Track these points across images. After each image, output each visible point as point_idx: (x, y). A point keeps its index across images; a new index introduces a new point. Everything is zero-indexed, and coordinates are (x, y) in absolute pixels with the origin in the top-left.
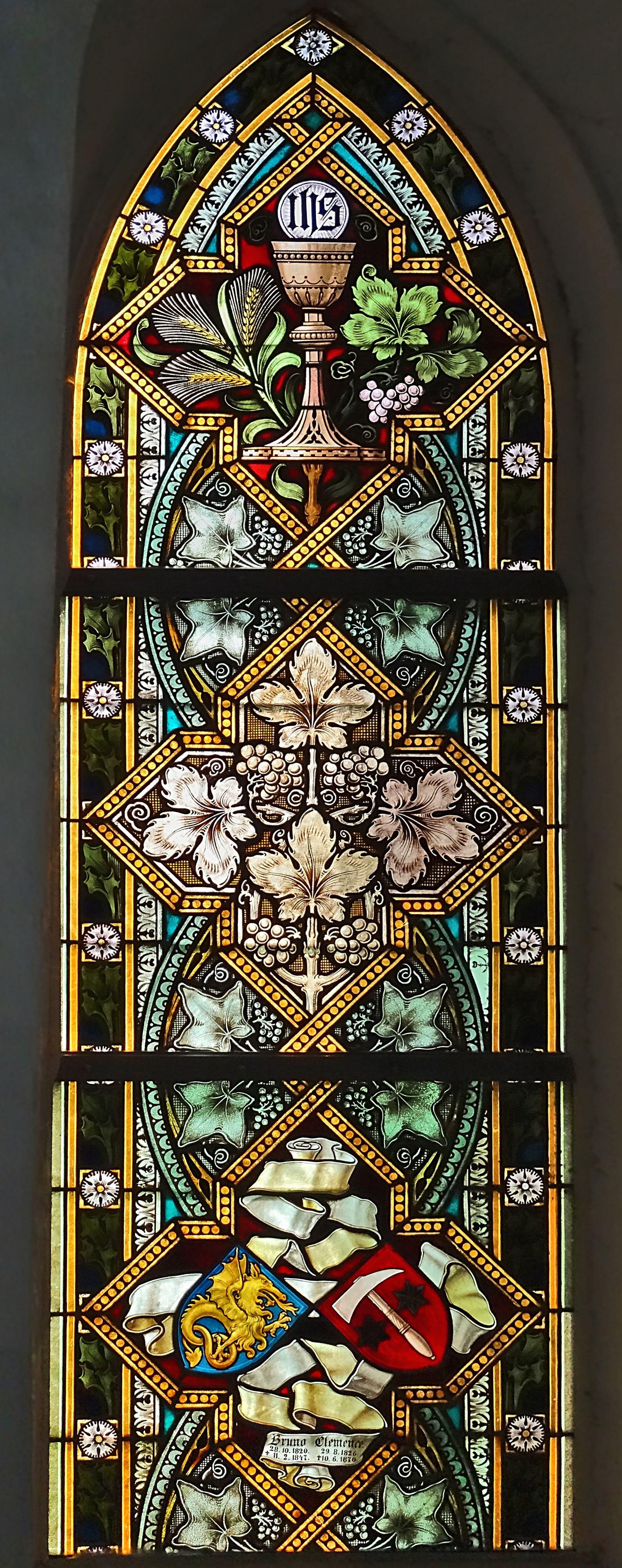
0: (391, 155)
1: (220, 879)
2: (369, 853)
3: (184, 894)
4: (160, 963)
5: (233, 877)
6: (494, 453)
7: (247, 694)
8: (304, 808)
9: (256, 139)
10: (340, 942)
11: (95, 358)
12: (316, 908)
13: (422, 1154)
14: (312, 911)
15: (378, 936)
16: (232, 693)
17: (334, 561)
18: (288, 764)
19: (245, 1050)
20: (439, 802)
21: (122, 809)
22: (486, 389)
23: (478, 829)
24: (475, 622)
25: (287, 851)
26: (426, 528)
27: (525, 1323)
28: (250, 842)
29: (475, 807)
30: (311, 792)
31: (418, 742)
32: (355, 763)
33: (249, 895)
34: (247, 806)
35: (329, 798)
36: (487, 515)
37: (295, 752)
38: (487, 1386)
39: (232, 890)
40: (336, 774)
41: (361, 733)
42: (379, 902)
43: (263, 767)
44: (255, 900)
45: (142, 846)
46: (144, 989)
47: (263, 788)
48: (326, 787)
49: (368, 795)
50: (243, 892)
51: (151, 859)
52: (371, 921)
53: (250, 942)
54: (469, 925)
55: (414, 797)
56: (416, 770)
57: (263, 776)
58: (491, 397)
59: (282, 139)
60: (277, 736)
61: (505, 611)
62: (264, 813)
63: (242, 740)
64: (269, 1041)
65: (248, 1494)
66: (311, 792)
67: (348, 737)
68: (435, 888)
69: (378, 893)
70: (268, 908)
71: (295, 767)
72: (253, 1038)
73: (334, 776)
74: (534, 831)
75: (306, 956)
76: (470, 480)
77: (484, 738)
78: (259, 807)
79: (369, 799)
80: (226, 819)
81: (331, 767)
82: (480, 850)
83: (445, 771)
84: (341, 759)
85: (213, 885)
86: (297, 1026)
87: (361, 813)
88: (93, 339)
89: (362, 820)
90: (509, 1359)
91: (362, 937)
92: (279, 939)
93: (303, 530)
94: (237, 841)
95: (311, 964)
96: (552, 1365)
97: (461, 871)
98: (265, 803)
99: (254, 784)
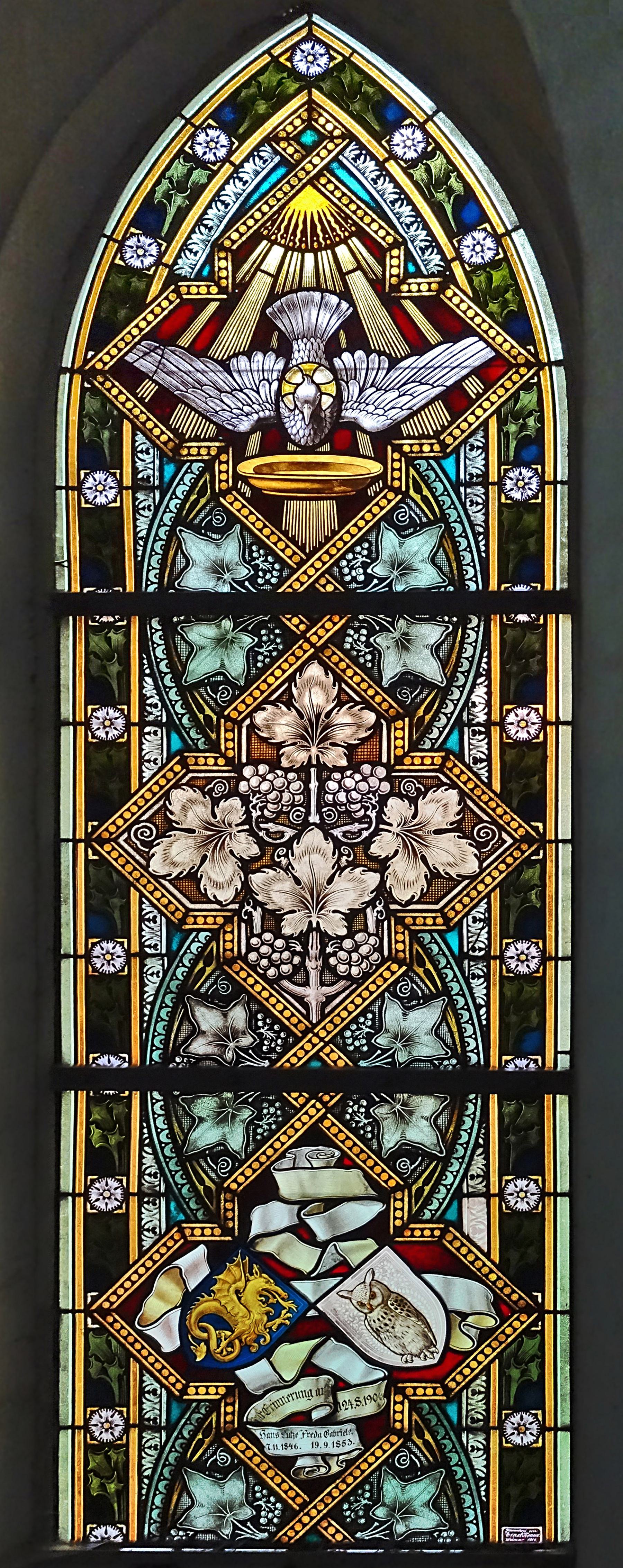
0: (389, 174)
1: (226, 895)
2: (370, 870)
3: (188, 910)
4: (157, 508)
5: (237, 894)
6: (494, 1421)
7: (250, 715)
8: (304, 826)
9: (251, 159)
10: (342, 955)
11: (89, 386)
12: (318, 923)
13: (421, 692)
14: (314, 925)
15: (380, 949)
16: (234, 715)
17: (337, 1059)
18: (289, 783)
19: (243, 591)
20: (440, 820)
21: (128, 829)
22: (487, 886)
23: (479, 846)
24: (478, 626)
25: (288, 868)
26: (426, 1497)
27: (522, 1323)
28: (254, 859)
29: (476, 825)
30: (313, 808)
31: (417, 761)
32: (357, 782)
33: (252, 910)
34: (251, 826)
35: (329, 816)
36: (487, 1484)
37: (296, 771)
38: (486, 942)
39: (236, 906)
40: (338, 791)
41: (362, 753)
42: (381, 916)
43: (265, 786)
44: (257, 915)
45: (148, 865)
46: (143, 534)
47: (265, 807)
48: (327, 805)
49: (368, 813)
50: (247, 907)
51: (156, 878)
52: (373, 935)
53: (253, 956)
54: (467, 1411)
55: (414, 816)
56: (417, 789)
57: (265, 795)
58: (493, 894)
59: (277, 159)
60: (279, 757)
61: (505, 982)
62: (267, 830)
63: (244, 760)
64: (268, 582)
65: (248, 540)
66: (313, 808)
67: (349, 757)
68: (437, 903)
69: (380, 908)
70: (271, 923)
71: (296, 786)
72: (253, 580)
73: (334, 794)
74: (535, 846)
75: (309, 968)
76: (470, 1449)
77: (484, 757)
78: (262, 826)
79: (369, 817)
80: (231, 838)
81: (332, 785)
82: (480, 866)
83: (446, 790)
84: (343, 778)
85: (219, 902)
86: (300, 1035)
87: (360, 831)
88: (87, 368)
89: (363, 837)
90: (506, 1360)
91: (364, 950)
92: (281, 952)
93: (301, 558)
94: (241, 859)
95: (314, 976)
96: (550, 890)
97: (459, 888)
98: (268, 821)
99: (257, 804)
